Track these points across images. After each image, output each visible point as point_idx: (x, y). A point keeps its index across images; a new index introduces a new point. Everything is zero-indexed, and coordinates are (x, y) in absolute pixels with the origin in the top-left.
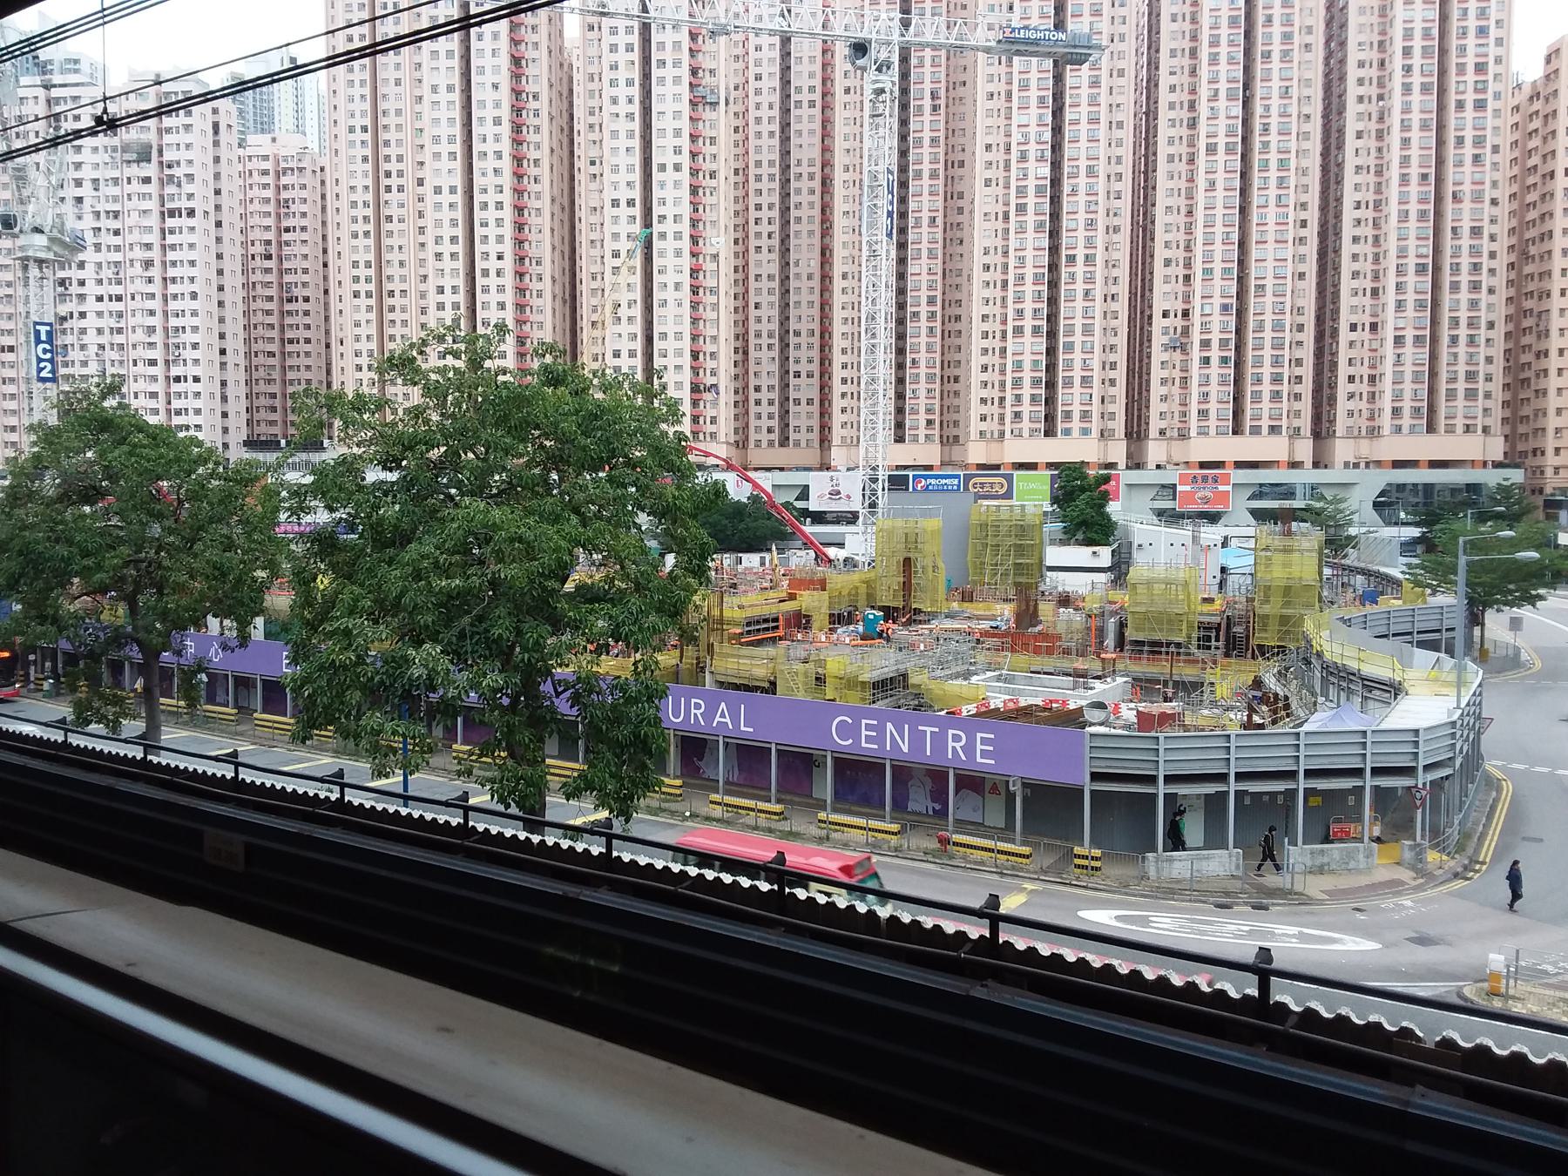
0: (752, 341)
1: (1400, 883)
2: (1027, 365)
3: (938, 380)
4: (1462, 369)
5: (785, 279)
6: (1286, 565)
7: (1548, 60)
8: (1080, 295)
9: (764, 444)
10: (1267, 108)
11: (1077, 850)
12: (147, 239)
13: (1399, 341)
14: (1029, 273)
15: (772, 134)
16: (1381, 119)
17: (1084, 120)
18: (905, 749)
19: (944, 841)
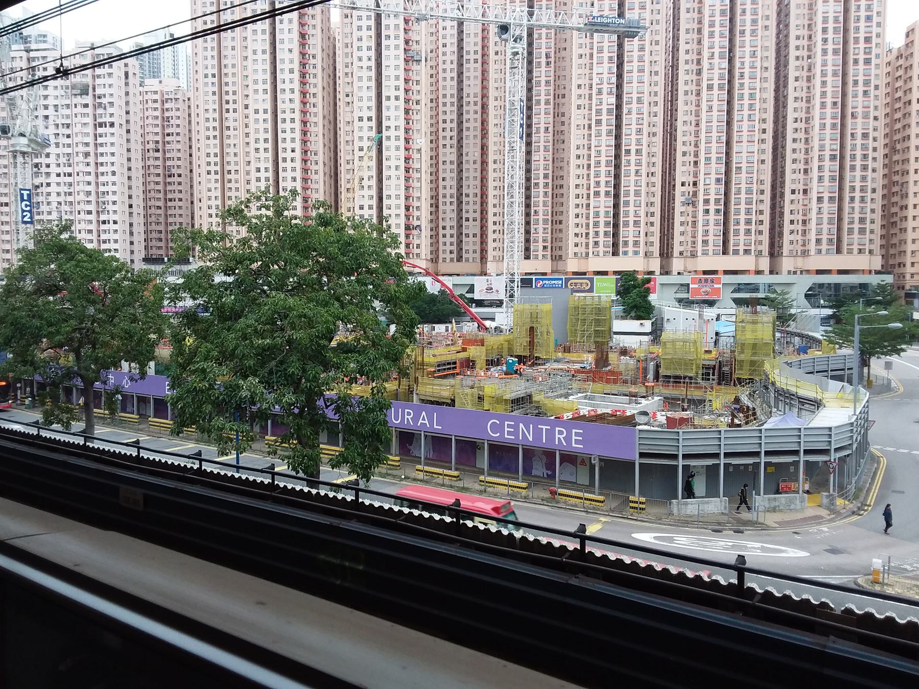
0: (441, 200)
1: (821, 517)
2: (602, 214)
3: (550, 223)
4: (857, 216)
5: (460, 164)
6: (754, 331)
7: (907, 35)
8: (633, 173)
9: (448, 260)
10: (743, 63)
11: (631, 498)
12: (86, 140)
13: (820, 200)
14: (603, 160)
15: (452, 78)
16: (809, 70)
17: (635, 70)
18: (531, 439)
19: (553, 493)
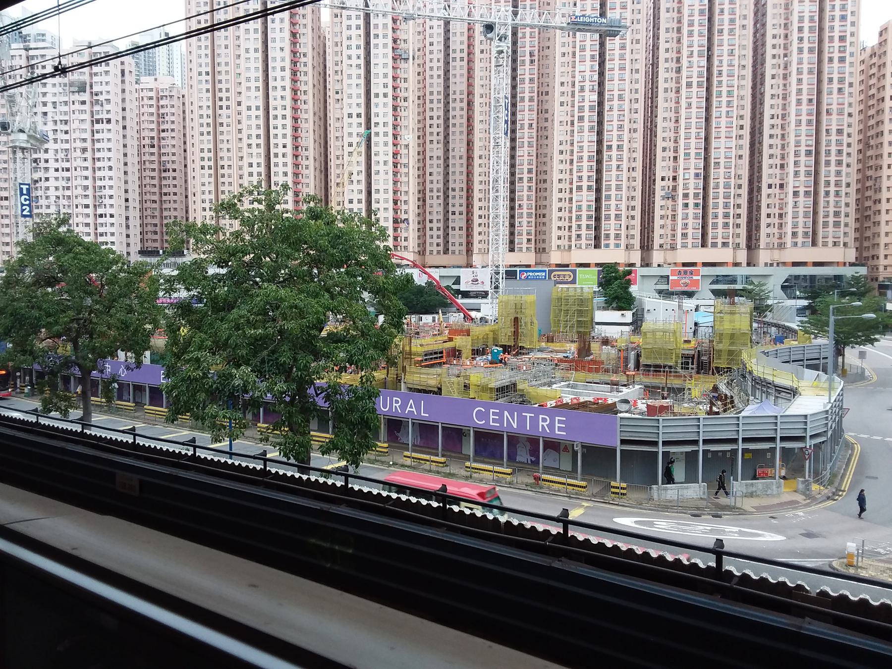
0: (428, 194)
1: (797, 502)
2: (584, 208)
3: (534, 216)
4: (831, 210)
5: (447, 159)
6: (732, 321)
7: (881, 34)
8: (614, 168)
9: (435, 253)
10: (721, 62)
11: (613, 483)
12: (84, 136)
13: (796, 194)
14: (585, 155)
15: (439, 76)
16: (786, 68)
17: (617, 68)
18: (515, 426)
19: (537, 479)
